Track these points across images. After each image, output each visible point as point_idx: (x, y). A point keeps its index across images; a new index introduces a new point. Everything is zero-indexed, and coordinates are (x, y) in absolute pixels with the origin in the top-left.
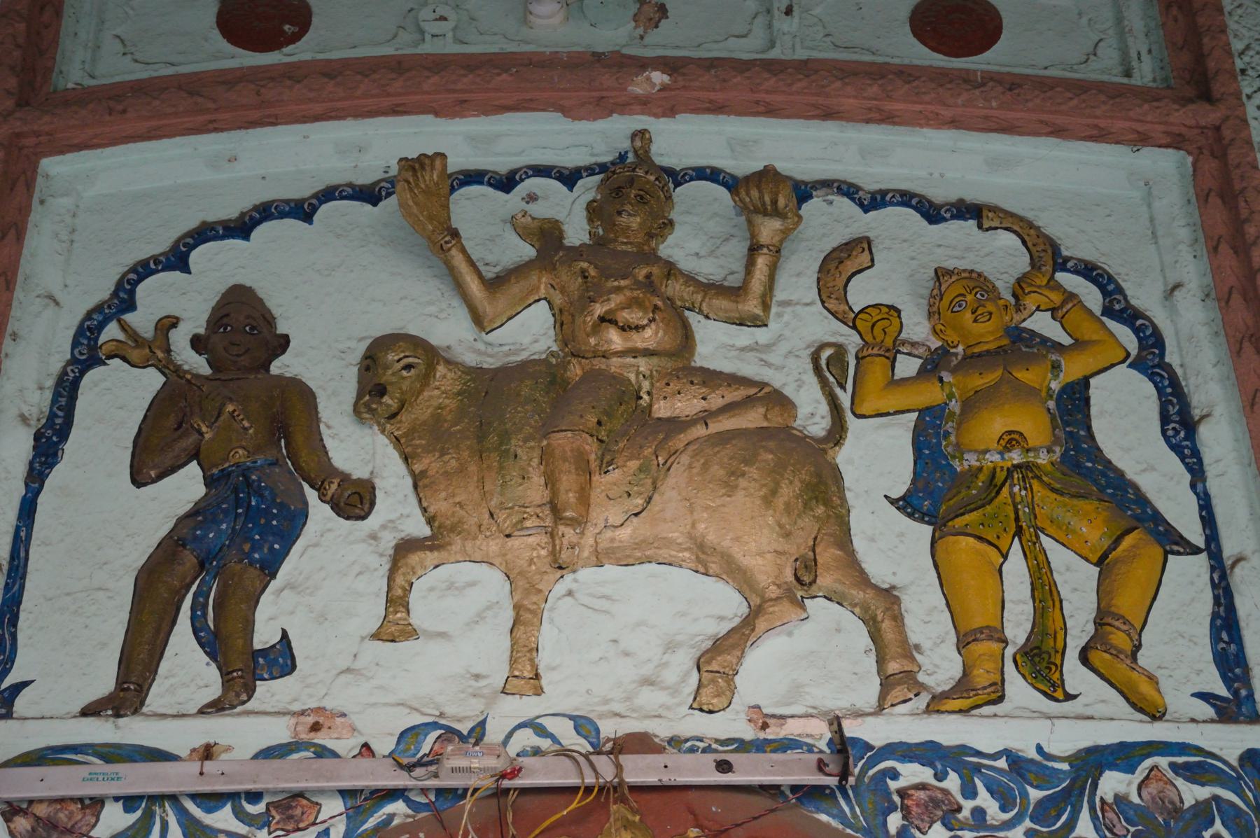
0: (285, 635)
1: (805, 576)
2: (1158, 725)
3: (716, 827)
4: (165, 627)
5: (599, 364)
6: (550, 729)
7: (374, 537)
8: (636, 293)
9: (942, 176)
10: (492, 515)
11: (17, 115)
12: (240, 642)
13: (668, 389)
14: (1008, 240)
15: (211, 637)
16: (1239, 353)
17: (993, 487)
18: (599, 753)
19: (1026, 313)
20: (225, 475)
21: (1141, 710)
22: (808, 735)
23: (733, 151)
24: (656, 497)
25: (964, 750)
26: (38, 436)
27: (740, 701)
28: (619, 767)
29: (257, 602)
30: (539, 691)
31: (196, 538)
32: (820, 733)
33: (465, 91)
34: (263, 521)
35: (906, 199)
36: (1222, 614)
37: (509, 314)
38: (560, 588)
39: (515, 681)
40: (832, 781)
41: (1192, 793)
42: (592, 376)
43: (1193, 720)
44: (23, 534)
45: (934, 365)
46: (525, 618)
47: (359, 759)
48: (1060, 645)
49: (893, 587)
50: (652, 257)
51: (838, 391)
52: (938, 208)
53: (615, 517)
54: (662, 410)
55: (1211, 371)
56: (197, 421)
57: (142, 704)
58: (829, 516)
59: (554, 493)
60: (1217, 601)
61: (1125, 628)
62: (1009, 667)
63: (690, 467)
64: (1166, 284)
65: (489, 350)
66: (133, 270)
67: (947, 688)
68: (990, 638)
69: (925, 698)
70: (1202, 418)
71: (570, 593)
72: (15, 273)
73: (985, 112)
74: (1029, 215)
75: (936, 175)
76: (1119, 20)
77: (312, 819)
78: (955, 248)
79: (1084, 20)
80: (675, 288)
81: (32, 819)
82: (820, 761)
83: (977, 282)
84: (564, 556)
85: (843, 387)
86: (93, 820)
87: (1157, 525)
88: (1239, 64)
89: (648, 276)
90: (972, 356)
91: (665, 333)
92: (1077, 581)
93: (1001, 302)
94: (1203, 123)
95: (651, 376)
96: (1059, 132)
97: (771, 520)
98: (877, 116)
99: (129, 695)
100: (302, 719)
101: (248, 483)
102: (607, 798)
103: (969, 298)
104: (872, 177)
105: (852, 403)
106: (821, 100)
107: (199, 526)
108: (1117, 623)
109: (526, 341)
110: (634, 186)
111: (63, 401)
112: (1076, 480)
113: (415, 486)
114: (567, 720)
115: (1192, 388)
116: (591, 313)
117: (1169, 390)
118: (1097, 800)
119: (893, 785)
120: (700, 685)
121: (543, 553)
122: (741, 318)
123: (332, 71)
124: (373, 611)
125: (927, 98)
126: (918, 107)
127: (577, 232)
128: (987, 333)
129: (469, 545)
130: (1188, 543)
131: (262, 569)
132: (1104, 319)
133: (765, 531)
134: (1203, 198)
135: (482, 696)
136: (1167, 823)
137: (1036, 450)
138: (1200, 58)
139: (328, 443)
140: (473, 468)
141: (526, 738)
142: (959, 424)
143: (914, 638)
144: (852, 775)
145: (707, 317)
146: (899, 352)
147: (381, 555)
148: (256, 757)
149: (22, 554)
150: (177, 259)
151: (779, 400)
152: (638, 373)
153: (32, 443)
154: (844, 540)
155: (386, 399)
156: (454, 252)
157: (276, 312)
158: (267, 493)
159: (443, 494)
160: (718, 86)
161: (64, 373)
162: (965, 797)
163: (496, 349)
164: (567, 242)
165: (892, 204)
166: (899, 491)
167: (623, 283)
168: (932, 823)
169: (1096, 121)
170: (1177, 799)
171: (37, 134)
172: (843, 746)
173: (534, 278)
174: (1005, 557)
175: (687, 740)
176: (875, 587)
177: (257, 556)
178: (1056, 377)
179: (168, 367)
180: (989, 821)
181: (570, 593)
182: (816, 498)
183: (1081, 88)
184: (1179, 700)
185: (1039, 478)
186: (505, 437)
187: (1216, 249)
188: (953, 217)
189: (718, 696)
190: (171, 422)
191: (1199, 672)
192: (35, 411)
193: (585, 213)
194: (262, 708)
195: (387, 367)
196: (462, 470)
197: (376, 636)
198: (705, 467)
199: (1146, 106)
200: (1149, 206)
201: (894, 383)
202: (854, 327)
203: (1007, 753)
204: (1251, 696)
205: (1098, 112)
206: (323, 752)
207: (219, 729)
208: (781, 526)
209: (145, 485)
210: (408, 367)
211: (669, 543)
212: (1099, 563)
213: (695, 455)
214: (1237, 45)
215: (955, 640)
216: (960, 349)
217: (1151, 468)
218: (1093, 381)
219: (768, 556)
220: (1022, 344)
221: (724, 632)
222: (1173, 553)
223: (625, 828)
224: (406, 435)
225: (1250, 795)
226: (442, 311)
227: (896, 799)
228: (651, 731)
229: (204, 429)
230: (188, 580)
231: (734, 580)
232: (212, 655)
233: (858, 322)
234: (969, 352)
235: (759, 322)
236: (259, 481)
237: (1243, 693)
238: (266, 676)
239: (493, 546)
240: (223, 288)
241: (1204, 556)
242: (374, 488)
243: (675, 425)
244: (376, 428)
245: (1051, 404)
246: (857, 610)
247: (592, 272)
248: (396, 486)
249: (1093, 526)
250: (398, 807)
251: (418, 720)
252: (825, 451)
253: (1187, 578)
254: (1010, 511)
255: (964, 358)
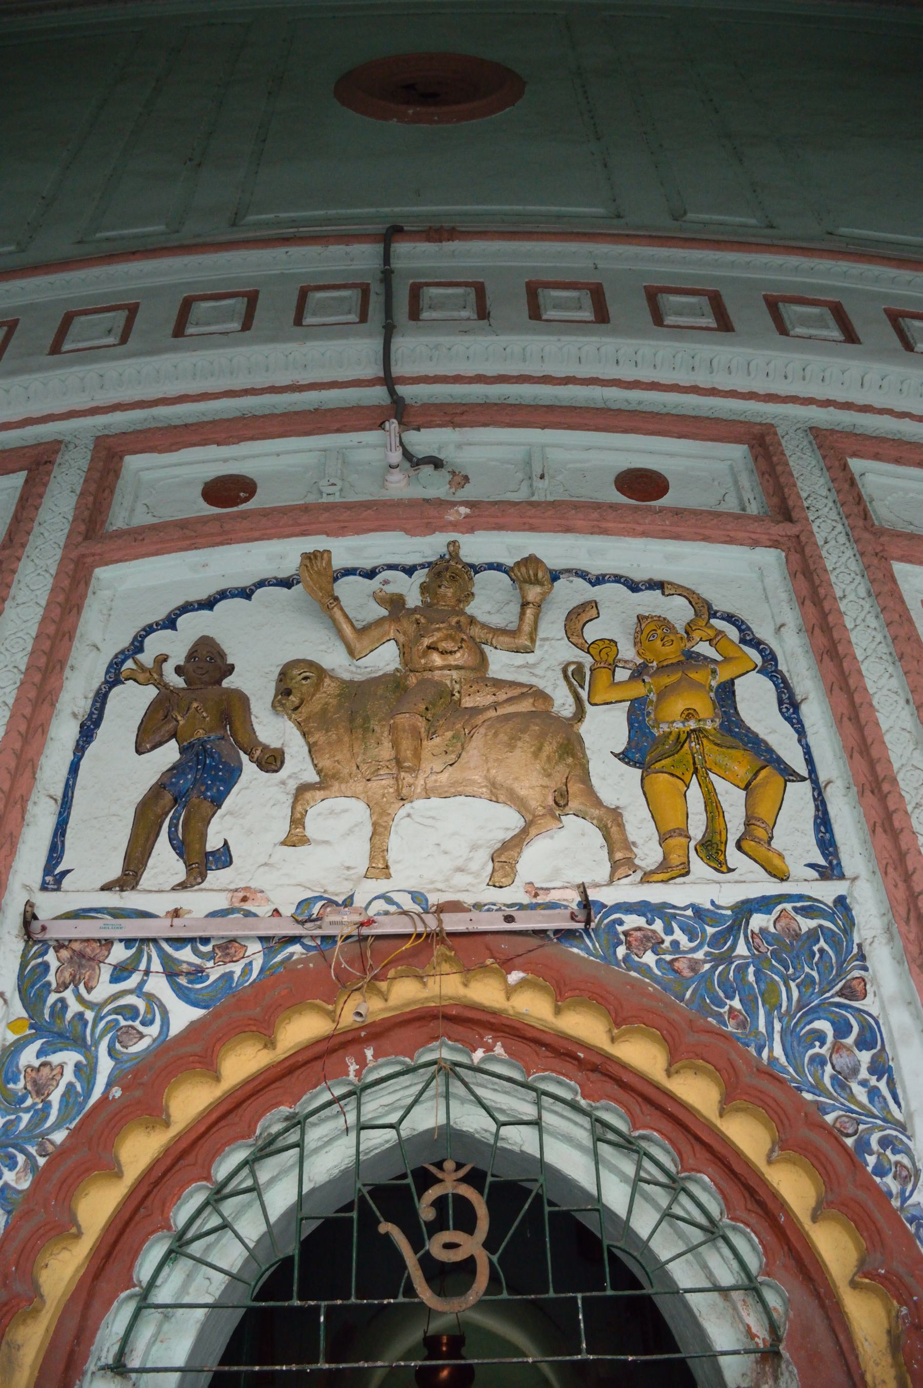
0: (226, 843)
1: (561, 801)
2: (784, 883)
3: (503, 958)
4: (152, 837)
5: (427, 675)
6: (396, 899)
7: (283, 783)
8: (450, 632)
9: (639, 566)
10: (358, 767)
11: (84, 544)
12: (197, 846)
13: (471, 690)
14: (681, 601)
15: (180, 845)
16: (821, 661)
17: (679, 743)
18: (427, 912)
19: (694, 642)
20: (191, 745)
21: (775, 876)
22: (564, 900)
23: (510, 552)
24: (464, 754)
25: (665, 905)
26: (82, 726)
27: (520, 881)
28: (440, 921)
29: (209, 823)
30: (388, 876)
31: (172, 784)
32: (573, 898)
33: (345, 521)
34: (213, 773)
35: (617, 579)
36: (821, 816)
37: (371, 648)
38: (402, 812)
39: (373, 870)
40: (581, 926)
41: (806, 924)
42: (421, 682)
43: (806, 880)
44: (71, 782)
45: (639, 673)
46: (379, 832)
47: (272, 918)
48: (724, 839)
49: (618, 808)
50: (462, 613)
51: (579, 690)
52: (637, 583)
53: (437, 766)
54: (467, 702)
55: (806, 673)
56: (175, 714)
57: (137, 884)
58: (576, 764)
59: (398, 752)
60: (817, 809)
61: (763, 825)
62: (693, 854)
63: (486, 735)
64: (775, 624)
65: (359, 671)
66: (144, 629)
67: (653, 868)
68: (680, 835)
69: (639, 874)
70: (802, 700)
71: (409, 815)
72: (75, 632)
73: (661, 527)
74: (693, 588)
75: (635, 565)
76: (736, 482)
77: (241, 955)
78: (649, 606)
79: (716, 483)
80: (475, 631)
81: (71, 952)
82: (572, 913)
83: (664, 623)
84: (405, 792)
85: (582, 687)
86: (106, 953)
87: (779, 765)
88: (806, 504)
89: (458, 622)
90: (663, 667)
91: (469, 655)
92: (733, 800)
93: (679, 636)
94: (789, 533)
95: (461, 682)
96: (706, 539)
97: (538, 767)
98: (597, 530)
99: (129, 878)
100: (236, 894)
101: (205, 750)
102: (432, 941)
103: (659, 631)
104: (596, 567)
105: (589, 697)
106: (563, 522)
107: (174, 776)
108: (758, 823)
109: (381, 665)
110: (450, 573)
111: (98, 705)
112: (730, 738)
113: (310, 751)
114: (407, 894)
115: (795, 683)
116: (422, 644)
117: (782, 685)
118: (749, 932)
119: (620, 929)
120: (494, 871)
121: (391, 790)
122: (517, 648)
123: (266, 513)
124: (282, 828)
125: (627, 520)
126: (622, 525)
127: (414, 599)
128: (671, 653)
129: (343, 786)
130: (798, 775)
131: (212, 802)
132: (741, 645)
133: (535, 773)
134: (793, 575)
135: (352, 880)
136: (792, 944)
137: (704, 720)
138: (784, 500)
139: (257, 727)
140: (346, 739)
141: (380, 905)
142: (656, 707)
143: (631, 838)
144: (727, 1105)
145: (496, 648)
146: (617, 666)
147: (288, 794)
148: (207, 916)
149: (70, 795)
150: (170, 623)
151: (541, 696)
152: (452, 680)
153: (79, 729)
154: (585, 778)
155: (292, 698)
156: (336, 609)
157: (226, 651)
158: (216, 756)
159: (327, 756)
160: (500, 515)
161: (100, 689)
162: (666, 934)
163: (363, 670)
164: (407, 606)
165: (609, 581)
166: (619, 749)
167: (441, 625)
168: (645, 951)
169: (728, 533)
170: (797, 929)
171: (93, 555)
172: (586, 904)
173: (386, 626)
174: (688, 787)
175: (485, 905)
176: (606, 807)
177: (209, 794)
178: (714, 678)
179: (160, 684)
180: (682, 948)
181: (409, 815)
182: (567, 753)
183: (718, 515)
184: (797, 869)
185: (707, 737)
186: (367, 719)
187: (803, 603)
188: (647, 589)
189: (505, 876)
190: (161, 715)
191: (808, 852)
192: (81, 711)
193: (419, 590)
194: (210, 887)
195: (292, 679)
196: (339, 740)
197: (284, 843)
198: (496, 734)
199: (756, 524)
200: (762, 581)
201: (614, 684)
202: (588, 652)
203: (692, 906)
204: (839, 864)
205: (729, 527)
206: (248, 914)
207: (183, 899)
208: (544, 769)
209: (143, 753)
210: (306, 678)
211: (473, 783)
212: (746, 788)
213: (489, 728)
214: (804, 495)
215: (658, 838)
216: (655, 664)
217: (773, 731)
218: (736, 681)
219: (537, 789)
220: (691, 658)
221: (509, 838)
222: (790, 781)
223: (446, 961)
224: (304, 721)
225: (840, 923)
226: (329, 648)
227: (622, 937)
228: (461, 900)
229: (179, 718)
230: (167, 809)
231: (515, 805)
232: (181, 855)
233: (591, 650)
234: (660, 665)
235: (529, 651)
236: (212, 748)
237: (835, 862)
238: (214, 868)
239: (359, 787)
240: (195, 638)
241: (808, 782)
242: (283, 753)
243: (476, 711)
244: (286, 717)
245: (712, 694)
246: (595, 822)
247: (423, 620)
248: (298, 752)
249: (741, 766)
250: (296, 949)
251: (310, 894)
252: (572, 726)
253: (799, 796)
254: (690, 757)
255: (658, 668)
